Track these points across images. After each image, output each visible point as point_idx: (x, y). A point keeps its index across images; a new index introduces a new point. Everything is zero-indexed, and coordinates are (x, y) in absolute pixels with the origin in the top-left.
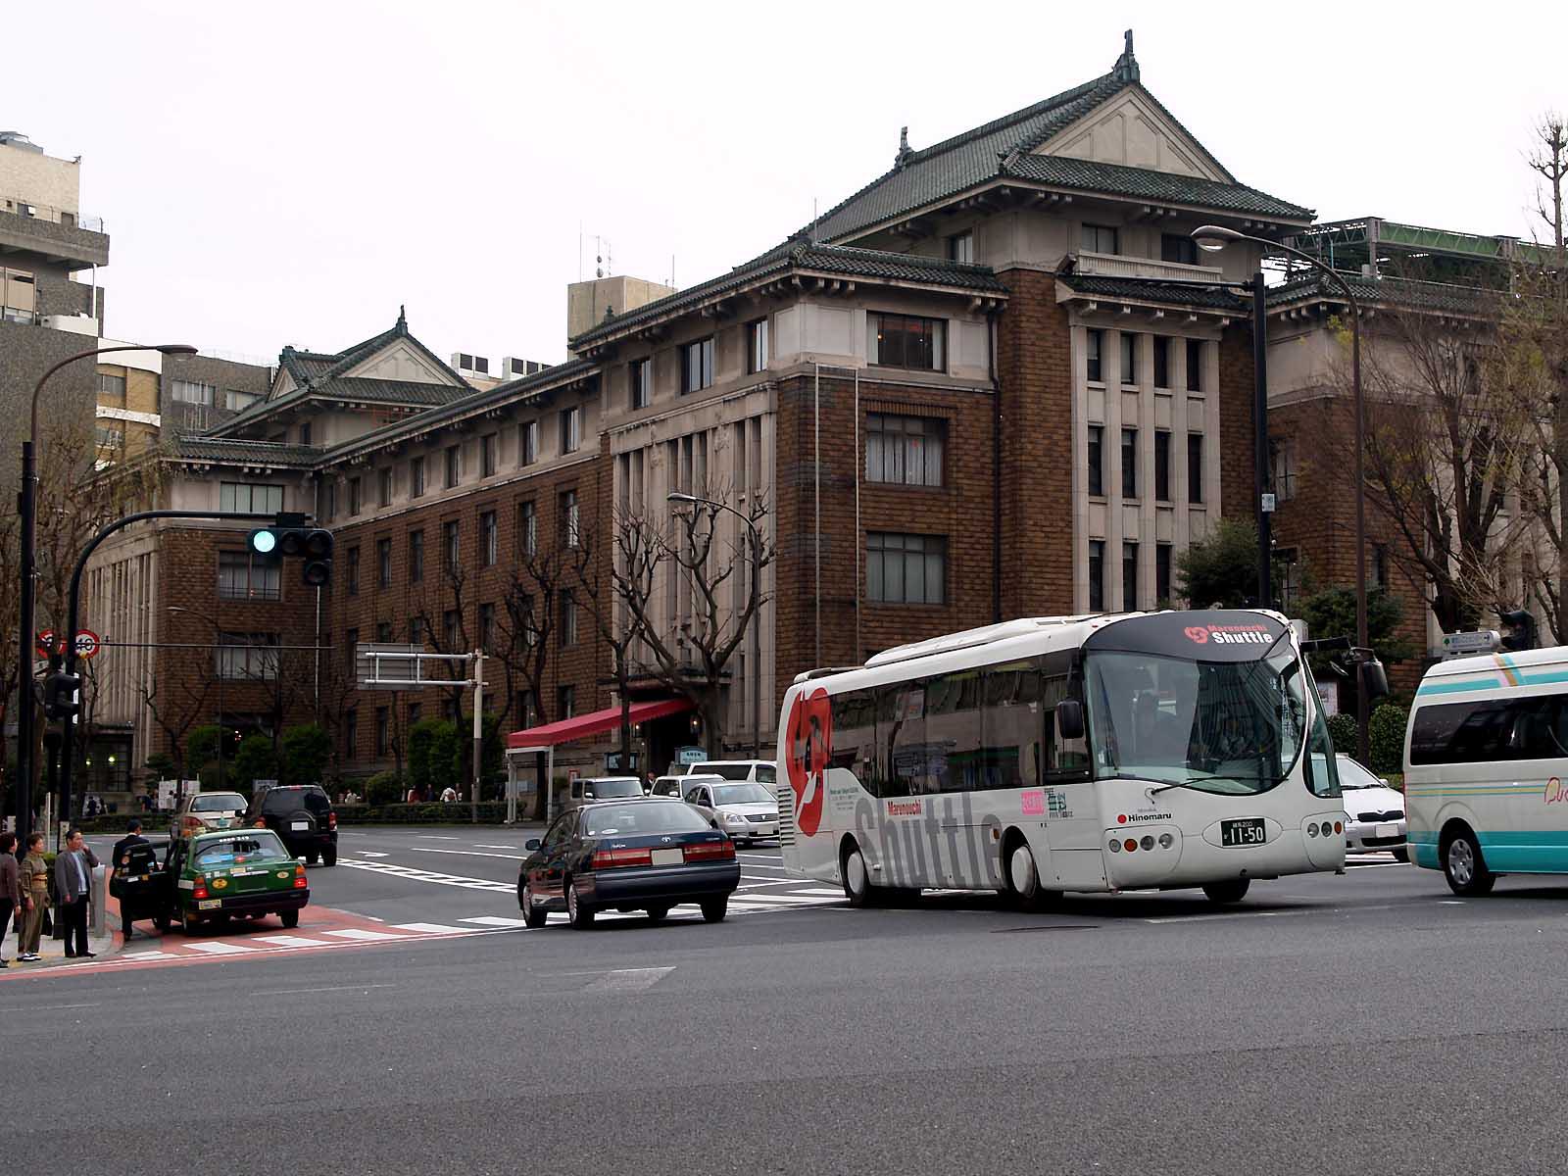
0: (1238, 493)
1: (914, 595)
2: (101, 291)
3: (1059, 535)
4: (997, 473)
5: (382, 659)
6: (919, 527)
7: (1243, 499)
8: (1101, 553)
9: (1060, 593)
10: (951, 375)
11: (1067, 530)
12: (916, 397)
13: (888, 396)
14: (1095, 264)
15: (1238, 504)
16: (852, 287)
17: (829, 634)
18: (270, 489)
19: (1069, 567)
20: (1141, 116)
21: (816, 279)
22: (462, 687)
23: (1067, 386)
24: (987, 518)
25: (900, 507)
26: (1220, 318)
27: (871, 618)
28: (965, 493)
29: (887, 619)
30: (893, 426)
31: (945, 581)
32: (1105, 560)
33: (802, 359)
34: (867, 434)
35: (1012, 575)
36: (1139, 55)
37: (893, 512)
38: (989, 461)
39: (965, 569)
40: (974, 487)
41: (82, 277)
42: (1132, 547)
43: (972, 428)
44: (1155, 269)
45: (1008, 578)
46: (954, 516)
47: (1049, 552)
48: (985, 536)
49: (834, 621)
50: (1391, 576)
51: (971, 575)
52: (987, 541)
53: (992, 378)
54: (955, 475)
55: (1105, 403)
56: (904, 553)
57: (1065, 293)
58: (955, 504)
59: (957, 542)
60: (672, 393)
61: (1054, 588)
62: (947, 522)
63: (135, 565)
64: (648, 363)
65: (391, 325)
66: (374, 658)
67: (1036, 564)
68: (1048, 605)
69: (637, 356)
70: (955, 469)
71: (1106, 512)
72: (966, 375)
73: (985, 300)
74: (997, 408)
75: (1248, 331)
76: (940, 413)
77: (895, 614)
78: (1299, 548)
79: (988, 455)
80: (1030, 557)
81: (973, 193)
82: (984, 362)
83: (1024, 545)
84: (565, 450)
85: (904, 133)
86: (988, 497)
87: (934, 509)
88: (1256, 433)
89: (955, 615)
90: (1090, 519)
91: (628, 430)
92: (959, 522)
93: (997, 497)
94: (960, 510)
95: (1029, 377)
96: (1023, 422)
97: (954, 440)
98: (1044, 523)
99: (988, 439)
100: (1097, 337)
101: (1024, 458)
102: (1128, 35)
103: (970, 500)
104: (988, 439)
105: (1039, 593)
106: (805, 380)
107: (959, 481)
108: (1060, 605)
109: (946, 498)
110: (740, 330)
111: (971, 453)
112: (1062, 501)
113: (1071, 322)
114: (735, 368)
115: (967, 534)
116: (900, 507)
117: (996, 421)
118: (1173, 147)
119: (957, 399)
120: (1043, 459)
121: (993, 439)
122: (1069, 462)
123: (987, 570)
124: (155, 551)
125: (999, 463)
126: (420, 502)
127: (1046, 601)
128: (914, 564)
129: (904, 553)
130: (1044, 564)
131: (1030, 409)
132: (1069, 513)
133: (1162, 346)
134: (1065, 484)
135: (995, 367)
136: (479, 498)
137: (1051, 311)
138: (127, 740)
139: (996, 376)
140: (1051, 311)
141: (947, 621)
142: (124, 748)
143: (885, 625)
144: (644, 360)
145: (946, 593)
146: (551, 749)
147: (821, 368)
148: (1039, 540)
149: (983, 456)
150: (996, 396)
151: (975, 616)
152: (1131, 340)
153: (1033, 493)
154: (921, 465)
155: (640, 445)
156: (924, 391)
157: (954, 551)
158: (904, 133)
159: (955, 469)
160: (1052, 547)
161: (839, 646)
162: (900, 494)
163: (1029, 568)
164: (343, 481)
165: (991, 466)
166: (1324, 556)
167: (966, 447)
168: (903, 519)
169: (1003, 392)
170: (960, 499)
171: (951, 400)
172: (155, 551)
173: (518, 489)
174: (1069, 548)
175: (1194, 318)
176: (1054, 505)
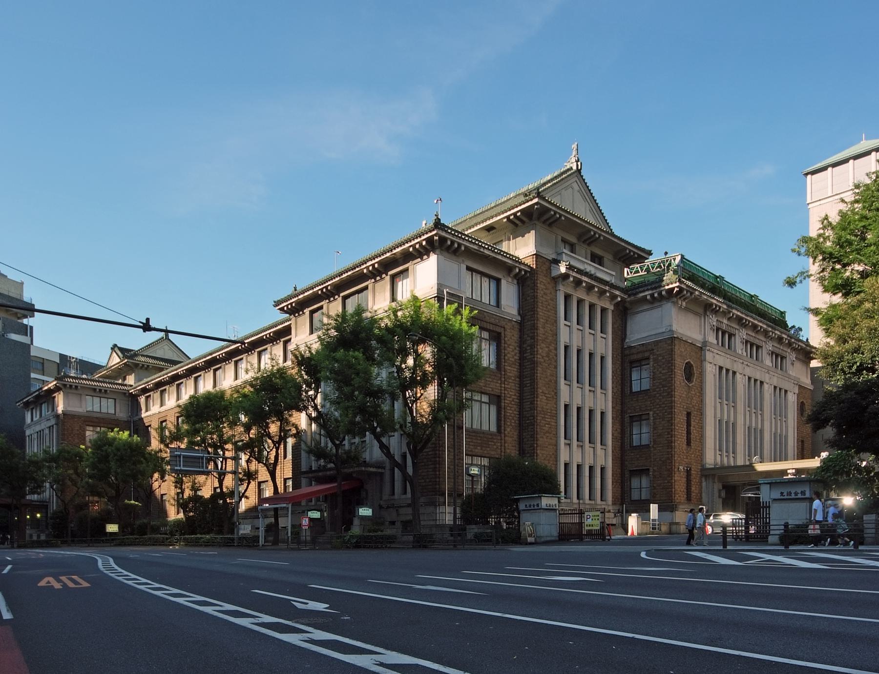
1: (485, 427)
2: (31, 328)
5: (184, 457)
12: (487, 319)
16: (463, 248)
19: (556, 416)
20: (580, 191)
23: (556, 322)
40: (512, 371)
41: (25, 321)
43: (511, 338)
53: (519, 314)
63: (47, 431)
66: (179, 456)
74: (521, 330)
76: (498, 330)
78: (651, 413)
88: (628, 359)
118: (591, 211)
122: (556, 361)
131: (541, 331)
138: (46, 507)
142: (44, 510)
146: (290, 506)
171: (503, 323)
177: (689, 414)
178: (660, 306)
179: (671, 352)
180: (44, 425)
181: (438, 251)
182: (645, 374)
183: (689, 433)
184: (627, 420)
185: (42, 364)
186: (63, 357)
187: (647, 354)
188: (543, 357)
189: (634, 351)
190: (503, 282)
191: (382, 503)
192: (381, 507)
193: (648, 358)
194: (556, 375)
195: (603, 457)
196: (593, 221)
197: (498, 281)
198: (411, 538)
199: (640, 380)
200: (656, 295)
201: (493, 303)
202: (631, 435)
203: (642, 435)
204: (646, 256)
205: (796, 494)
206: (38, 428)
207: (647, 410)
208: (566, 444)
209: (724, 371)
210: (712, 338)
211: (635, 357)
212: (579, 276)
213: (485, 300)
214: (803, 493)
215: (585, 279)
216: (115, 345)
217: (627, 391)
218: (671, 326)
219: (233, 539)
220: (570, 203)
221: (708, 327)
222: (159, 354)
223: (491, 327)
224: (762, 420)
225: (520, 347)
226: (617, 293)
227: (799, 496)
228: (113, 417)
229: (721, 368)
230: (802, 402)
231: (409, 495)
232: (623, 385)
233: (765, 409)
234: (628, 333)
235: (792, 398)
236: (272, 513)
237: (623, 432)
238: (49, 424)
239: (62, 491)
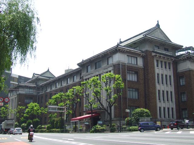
1: (134, 98)
4: (145, 80)
5: (52, 107)
14: (157, 50)
16: (125, 51)
18: (132, 58)
19: (155, 94)
20: (160, 32)
22: (62, 112)
23: (154, 68)
31: (138, 95)
33: (118, 61)
36: (159, 24)
42: (167, 92)
43: (141, 73)
44: (164, 52)
53: (143, 66)
57: (153, 54)
60: (94, 69)
63: (14, 99)
64: (90, 66)
65: (47, 70)
66: (50, 107)
69: (88, 65)
72: (140, 65)
73: (143, 55)
74: (144, 71)
75: (177, 61)
76: (137, 71)
81: (140, 40)
82: (142, 64)
84: (74, 81)
85: (120, 39)
88: (178, 76)
91: (87, 75)
93: (145, 83)
102: (158, 21)
103: (141, 83)
106: (119, 64)
110: (107, 59)
114: (105, 64)
117: (144, 72)
124: (112, 70)
126: (52, 90)
128: (134, 93)
132: (155, 86)
136: (61, 89)
144: (89, 66)
146: (79, 121)
150: (144, 69)
155: (89, 77)
158: (120, 39)
164: (41, 88)
172: (112, 70)
173: (66, 87)
175: (170, 59)
178: (186, 61)
180: (14, 97)
181: (118, 52)
182: (184, 80)
185: (13, 79)
186: (19, 76)
190: (138, 58)
191: (105, 120)
192: (105, 121)
193: (184, 76)
194: (155, 82)
195: (172, 105)
196: (165, 40)
197: (137, 58)
198: (150, 119)
199: (182, 82)
201: (135, 63)
202: (181, 98)
203: (184, 98)
206: (12, 98)
208: (159, 102)
212: (160, 55)
213: (133, 63)
215: (161, 56)
216: (34, 73)
219: (64, 130)
220: (156, 36)
222: (46, 76)
223: (135, 70)
225: (144, 75)
226: (173, 58)
228: (33, 94)
231: (109, 118)
234: (178, 68)
236: (75, 123)
238: (15, 97)
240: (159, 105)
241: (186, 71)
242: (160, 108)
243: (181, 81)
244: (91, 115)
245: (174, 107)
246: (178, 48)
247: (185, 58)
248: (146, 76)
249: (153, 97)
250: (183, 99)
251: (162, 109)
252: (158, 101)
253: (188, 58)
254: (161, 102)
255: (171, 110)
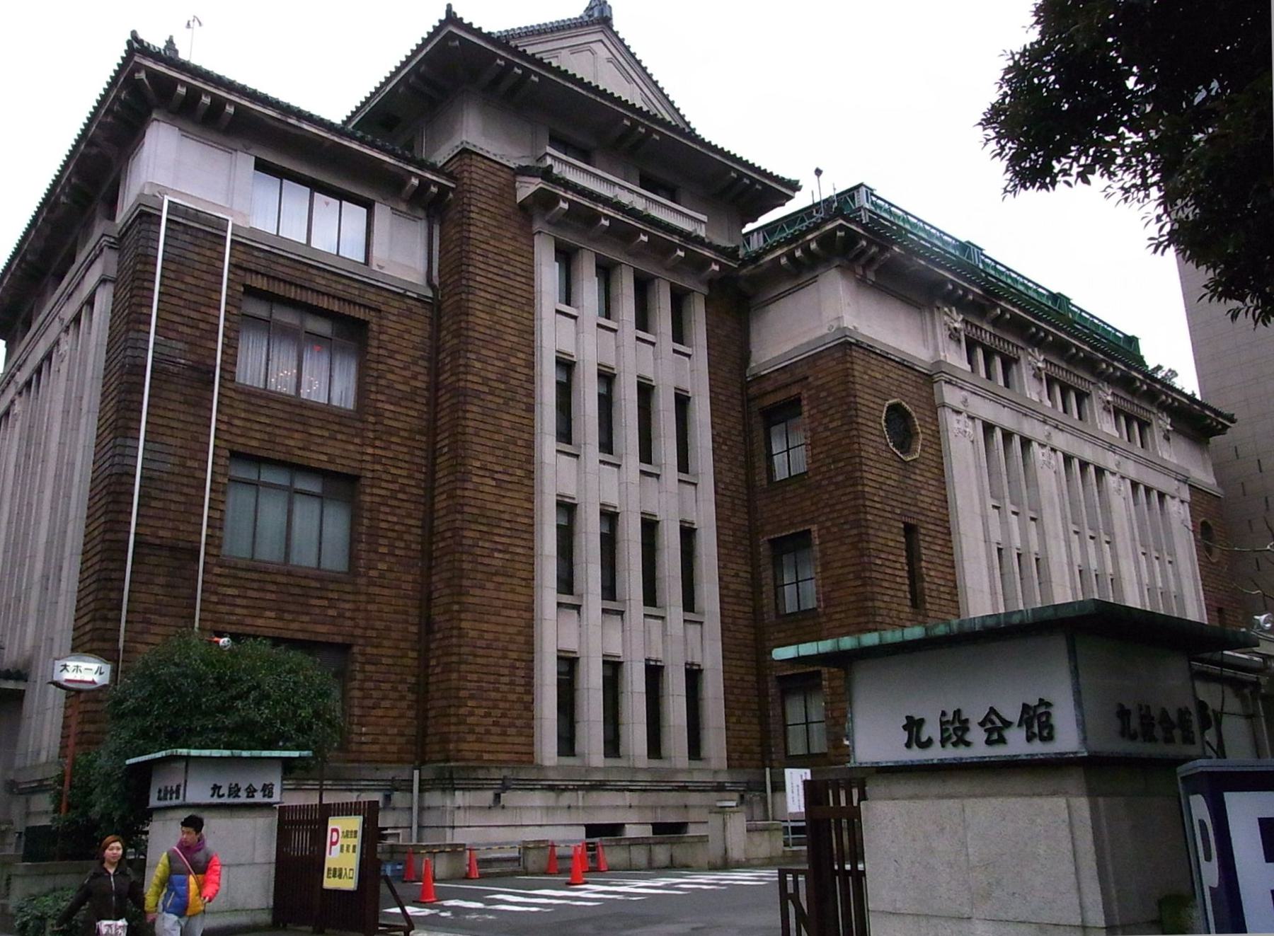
0: (730, 470)
1: (304, 557)
3: (516, 487)
4: (433, 403)
6: (317, 458)
7: (736, 477)
8: (610, 390)
9: (518, 566)
10: (375, 268)
11: (526, 482)
13: (280, 271)
15: (731, 483)
17: (152, 599)
19: (528, 531)
21: (176, 82)
24: (418, 460)
25: (288, 425)
26: (709, 261)
27: (227, 581)
28: (386, 422)
29: (255, 585)
30: (287, 317)
31: (353, 540)
32: (577, 529)
34: (240, 322)
35: (449, 534)
37: (277, 431)
38: (424, 386)
39: (383, 525)
42: (650, 527)
43: (402, 340)
45: (444, 539)
46: (370, 451)
47: (501, 508)
48: (413, 483)
49: (161, 580)
50: (923, 564)
51: (390, 534)
52: (415, 491)
54: (373, 396)
55: (577, 333)
56: (292, 493)
58: (371, 435)
59: (372, 486)
61: (507, 557)
62: (359, 457)
67: (484, 521)
68: (500, 579)
70: (375, 343)
71: (578, 465)
74: (436, 325)
77: (268, 578)
78: (814, 528)
79: (420, 377)
80: (475, 511)
83: (467, 493)
86: (420, 433)
87: (339, 436)
88: (754, 406)
89: (363, 589)
90: (557, 473)
92: (376, 459)
94: (378, 443)
95: (478, 278)
96: (471, 333)
97: (375, 351)
98: (497, 468)
99: (422, 358)
100: (566, 256)
101: (470, 377)
103: (391, 431)
104: (422, 358)
105: (486, 561)
107: (379, 405)
108: (515, 581)
109: (359, 425)
111: (397, 371)
112: (520, 443)
113: (537, 226)
115: (389, 478)
116: (288, 425)
119: (381, 299)
120: (496, 384)
121: (429, 360)
122: (531, 394)
123: (414, 530)
125: (437, 390)
127: (496, 574)
129: (292, 493)
130: (495, 522)
131: (480, 317)
132: (530, 459)
133: (643, 287)
134: (525, 421)
135: (435, 272)
137: (510, 210)
139: (436, 282)
140: (510, 210)
141: (351, 597)
143: (250, 593)
145: (353, 557)
147: (173, 207)
148: (487, 489)
149: (415, 378)
151: (394, 592)
152: (606, 271)
153: (481, 426)
154: (326, 382)
156: (334, 278)
157: (368, 499)
159: (373, 389)
160: (506, 501)
161: (167, 620)
162: (288, 409)
163: (473, 526)
165: (426, 393)
166: (855, 532)
167: (390, 361)
168: (292, 443)
169: (444, 304)
170: (378, 427)
171: (371, 297)
174: (529, 506)
176: (511, 447)
177: (910, 530)
178: (814, 279)
179: (846, 378)
182: (799, 438)
183: (914, 576)
184: (764, 549)
187: (794, 390)
188: (485, 382)
189: (768, 386)
194: (528, 427)
199: (788, 456)
200: (798, 253)
202: (778, 587)
204: (789, 193)
205: (995, 728)
207: (806, 522)
209: (998, 435)
210: (956, 358)
211: (769, 401)
214: (1037, 720)
217: (761, 479)
218: (839, 318)
220: (590, 65)
221: (942, 334)
224: (1115, 557)
227: (1017, 744)
229: (988, 428)
230: (1204, 523)
232: (749, 466)
233: (1117, 530)
235: (1179, 512)
237: (755, 583)
239: (287, 740)
240: (554, 633)
241: (813, 360)
242: (569, 665)
243: (777, 446)
244: (128, 762)
245: (712, 660)
246: (765, 189)
247: (806, 250)
248: (441, 381)
249: (498, 560)
250: (789, 591)
251: (592, 679)
252: (548, 594)
253: (827, 241)
254: (578, 608)
255: (675, 686)
